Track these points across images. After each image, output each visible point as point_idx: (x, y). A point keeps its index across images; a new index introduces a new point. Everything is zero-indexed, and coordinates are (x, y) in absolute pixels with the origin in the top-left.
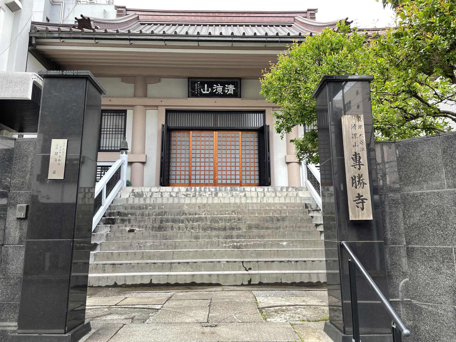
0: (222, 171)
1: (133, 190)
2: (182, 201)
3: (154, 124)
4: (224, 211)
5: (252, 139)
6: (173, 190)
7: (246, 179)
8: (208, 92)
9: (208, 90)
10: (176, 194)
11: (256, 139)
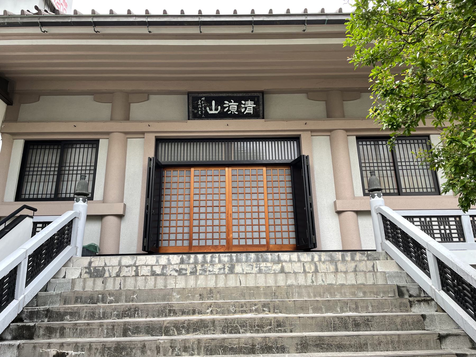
0: (239, 225)
1: (90, 263)
2: (171, 284)
3: (136, 159)
4: (248, 306)
5: (282, 178)
6: (157, 261)
7: (275, 238)
8: (217, 112)
9: (216, 109)
10: (163, 269)
11: (288, 178)
